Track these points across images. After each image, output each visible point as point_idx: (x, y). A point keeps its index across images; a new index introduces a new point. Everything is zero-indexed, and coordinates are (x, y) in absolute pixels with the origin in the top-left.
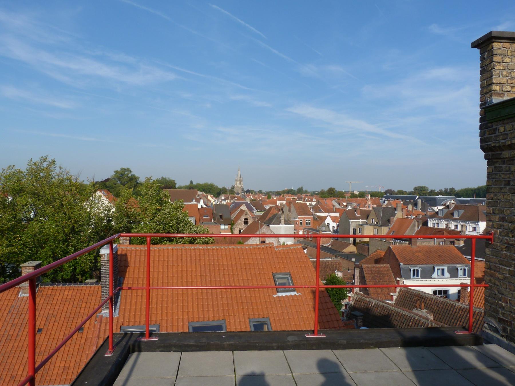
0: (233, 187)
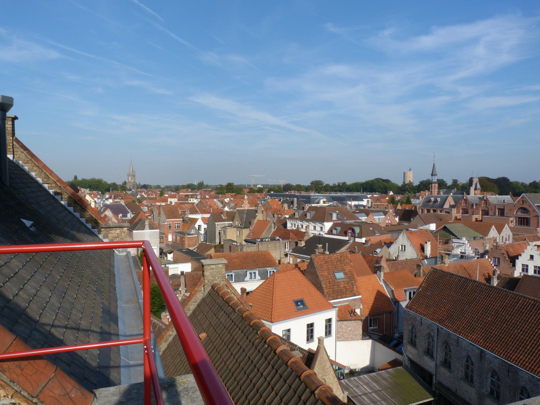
0: (125, 183)
